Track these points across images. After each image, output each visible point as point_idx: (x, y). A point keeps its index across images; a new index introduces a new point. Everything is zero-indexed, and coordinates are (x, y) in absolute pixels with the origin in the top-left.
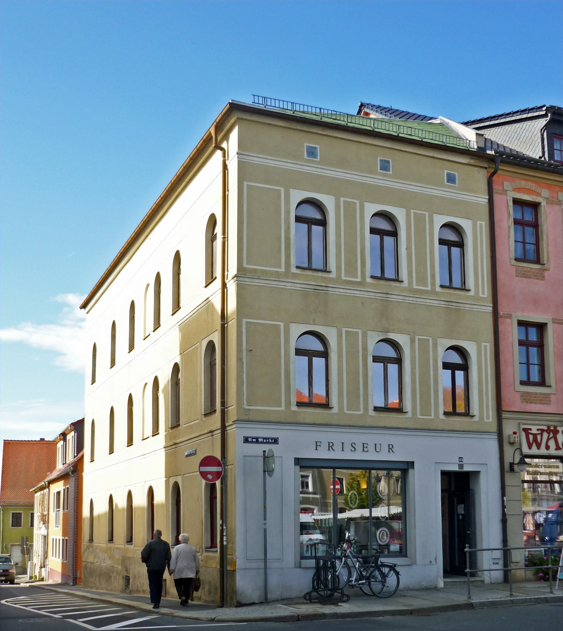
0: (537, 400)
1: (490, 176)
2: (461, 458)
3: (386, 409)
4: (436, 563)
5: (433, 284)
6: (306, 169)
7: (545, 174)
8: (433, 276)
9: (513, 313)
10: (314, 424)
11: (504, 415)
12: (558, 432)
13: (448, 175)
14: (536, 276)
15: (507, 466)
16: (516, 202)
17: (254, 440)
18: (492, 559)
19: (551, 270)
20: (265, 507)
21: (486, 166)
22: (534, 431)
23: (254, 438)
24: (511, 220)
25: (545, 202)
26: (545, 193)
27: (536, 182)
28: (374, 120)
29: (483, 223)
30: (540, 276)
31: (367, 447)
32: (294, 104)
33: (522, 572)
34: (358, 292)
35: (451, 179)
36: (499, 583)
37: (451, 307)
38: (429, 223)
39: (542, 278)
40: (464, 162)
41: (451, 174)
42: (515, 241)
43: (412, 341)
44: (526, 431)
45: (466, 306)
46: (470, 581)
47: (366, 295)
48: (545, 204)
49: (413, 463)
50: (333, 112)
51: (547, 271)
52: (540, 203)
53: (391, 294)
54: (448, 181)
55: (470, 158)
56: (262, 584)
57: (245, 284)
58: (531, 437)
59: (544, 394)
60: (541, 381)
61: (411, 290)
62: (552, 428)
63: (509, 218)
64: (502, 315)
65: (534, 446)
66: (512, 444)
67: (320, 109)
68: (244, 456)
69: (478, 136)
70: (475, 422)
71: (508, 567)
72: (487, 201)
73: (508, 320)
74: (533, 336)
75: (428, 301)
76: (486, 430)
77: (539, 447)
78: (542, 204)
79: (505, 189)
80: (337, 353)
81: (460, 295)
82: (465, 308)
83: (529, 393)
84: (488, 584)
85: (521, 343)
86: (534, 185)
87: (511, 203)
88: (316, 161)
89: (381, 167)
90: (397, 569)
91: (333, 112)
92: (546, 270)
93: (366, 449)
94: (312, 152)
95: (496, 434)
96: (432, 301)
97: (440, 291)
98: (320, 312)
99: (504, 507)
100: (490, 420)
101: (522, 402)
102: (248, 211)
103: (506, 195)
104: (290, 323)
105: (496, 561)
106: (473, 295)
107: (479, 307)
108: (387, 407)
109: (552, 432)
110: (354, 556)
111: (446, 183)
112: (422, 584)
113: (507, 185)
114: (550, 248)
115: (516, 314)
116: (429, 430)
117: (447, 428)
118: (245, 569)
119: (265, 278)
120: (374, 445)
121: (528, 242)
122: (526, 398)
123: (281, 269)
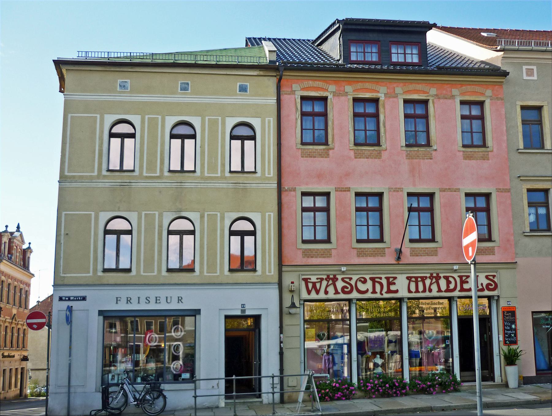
0: (376, 254)
2: (243, 304)
3: (181, 270)
4: (218, 388)
6: (118, 98)
7: (346, 74)
10: (116, 285)
11: (284, 269)
12: (337, 279)
14: (319, 155)
17: (67, 299)
20: (70, 348)
22: (314, 279)
23: (67, 297)
26: (332, 88)
27: (324, 81)
28: (175, 54)
29: (272, 119)
30: (326, 155)
31: (159, 300)
32: (110, 53)
34: (157, 184)
35: (243, 89)
37: (239, 187)
39: (328, 156)
40: (255, 74)
42: (462, 132)
43: (202, 217)
44: (306, 281)
45: (252, 185)
47: (163, 185)
49: (200, 310)
50: (141, 54)
52: (327, 97)
53: (185, 183)
54: (240, 91)
56: (66, 405)
57: (65, 187)
58: (310, 286)
59: (326, 249)
61: (203, 178)
63: (296, 112)
65: (313, 292)
66: (291, 291)
67: (130, 53)
69: (271, 53)
70: (258, 276)
73: (293, 193)
75: (218, 185)
76: (268, 281)
77: (318, 292)
80: (137, 231)
81: (246, 177)
82: (252, 187)
83: (310, 250)
84: (266, 404)
88: (127, 91)
89: (181, 88)
90: (165, 393)
91: (141, 54)
92: (330, 149)
93: (158, 302)
94: (123, 86)
95: (277, 284)
96: (221, 185)
97: (229, 176)
98: (124, 202)
100: (272, 273)
101: (304, 257)
102: (71, 134)
103: (294, 94)
107: (264, 185)
108: (181, 268)
110: (130, 383)
111: (238, 92)
112: (205, 404)
113: (295, 87)
114: (335, 131)
117: (231, 282)
118: (56, 393)
119: (81, 181)
120: (138, 298)
121: (475, 131)
122: (307, 254)
123: (94, 173)
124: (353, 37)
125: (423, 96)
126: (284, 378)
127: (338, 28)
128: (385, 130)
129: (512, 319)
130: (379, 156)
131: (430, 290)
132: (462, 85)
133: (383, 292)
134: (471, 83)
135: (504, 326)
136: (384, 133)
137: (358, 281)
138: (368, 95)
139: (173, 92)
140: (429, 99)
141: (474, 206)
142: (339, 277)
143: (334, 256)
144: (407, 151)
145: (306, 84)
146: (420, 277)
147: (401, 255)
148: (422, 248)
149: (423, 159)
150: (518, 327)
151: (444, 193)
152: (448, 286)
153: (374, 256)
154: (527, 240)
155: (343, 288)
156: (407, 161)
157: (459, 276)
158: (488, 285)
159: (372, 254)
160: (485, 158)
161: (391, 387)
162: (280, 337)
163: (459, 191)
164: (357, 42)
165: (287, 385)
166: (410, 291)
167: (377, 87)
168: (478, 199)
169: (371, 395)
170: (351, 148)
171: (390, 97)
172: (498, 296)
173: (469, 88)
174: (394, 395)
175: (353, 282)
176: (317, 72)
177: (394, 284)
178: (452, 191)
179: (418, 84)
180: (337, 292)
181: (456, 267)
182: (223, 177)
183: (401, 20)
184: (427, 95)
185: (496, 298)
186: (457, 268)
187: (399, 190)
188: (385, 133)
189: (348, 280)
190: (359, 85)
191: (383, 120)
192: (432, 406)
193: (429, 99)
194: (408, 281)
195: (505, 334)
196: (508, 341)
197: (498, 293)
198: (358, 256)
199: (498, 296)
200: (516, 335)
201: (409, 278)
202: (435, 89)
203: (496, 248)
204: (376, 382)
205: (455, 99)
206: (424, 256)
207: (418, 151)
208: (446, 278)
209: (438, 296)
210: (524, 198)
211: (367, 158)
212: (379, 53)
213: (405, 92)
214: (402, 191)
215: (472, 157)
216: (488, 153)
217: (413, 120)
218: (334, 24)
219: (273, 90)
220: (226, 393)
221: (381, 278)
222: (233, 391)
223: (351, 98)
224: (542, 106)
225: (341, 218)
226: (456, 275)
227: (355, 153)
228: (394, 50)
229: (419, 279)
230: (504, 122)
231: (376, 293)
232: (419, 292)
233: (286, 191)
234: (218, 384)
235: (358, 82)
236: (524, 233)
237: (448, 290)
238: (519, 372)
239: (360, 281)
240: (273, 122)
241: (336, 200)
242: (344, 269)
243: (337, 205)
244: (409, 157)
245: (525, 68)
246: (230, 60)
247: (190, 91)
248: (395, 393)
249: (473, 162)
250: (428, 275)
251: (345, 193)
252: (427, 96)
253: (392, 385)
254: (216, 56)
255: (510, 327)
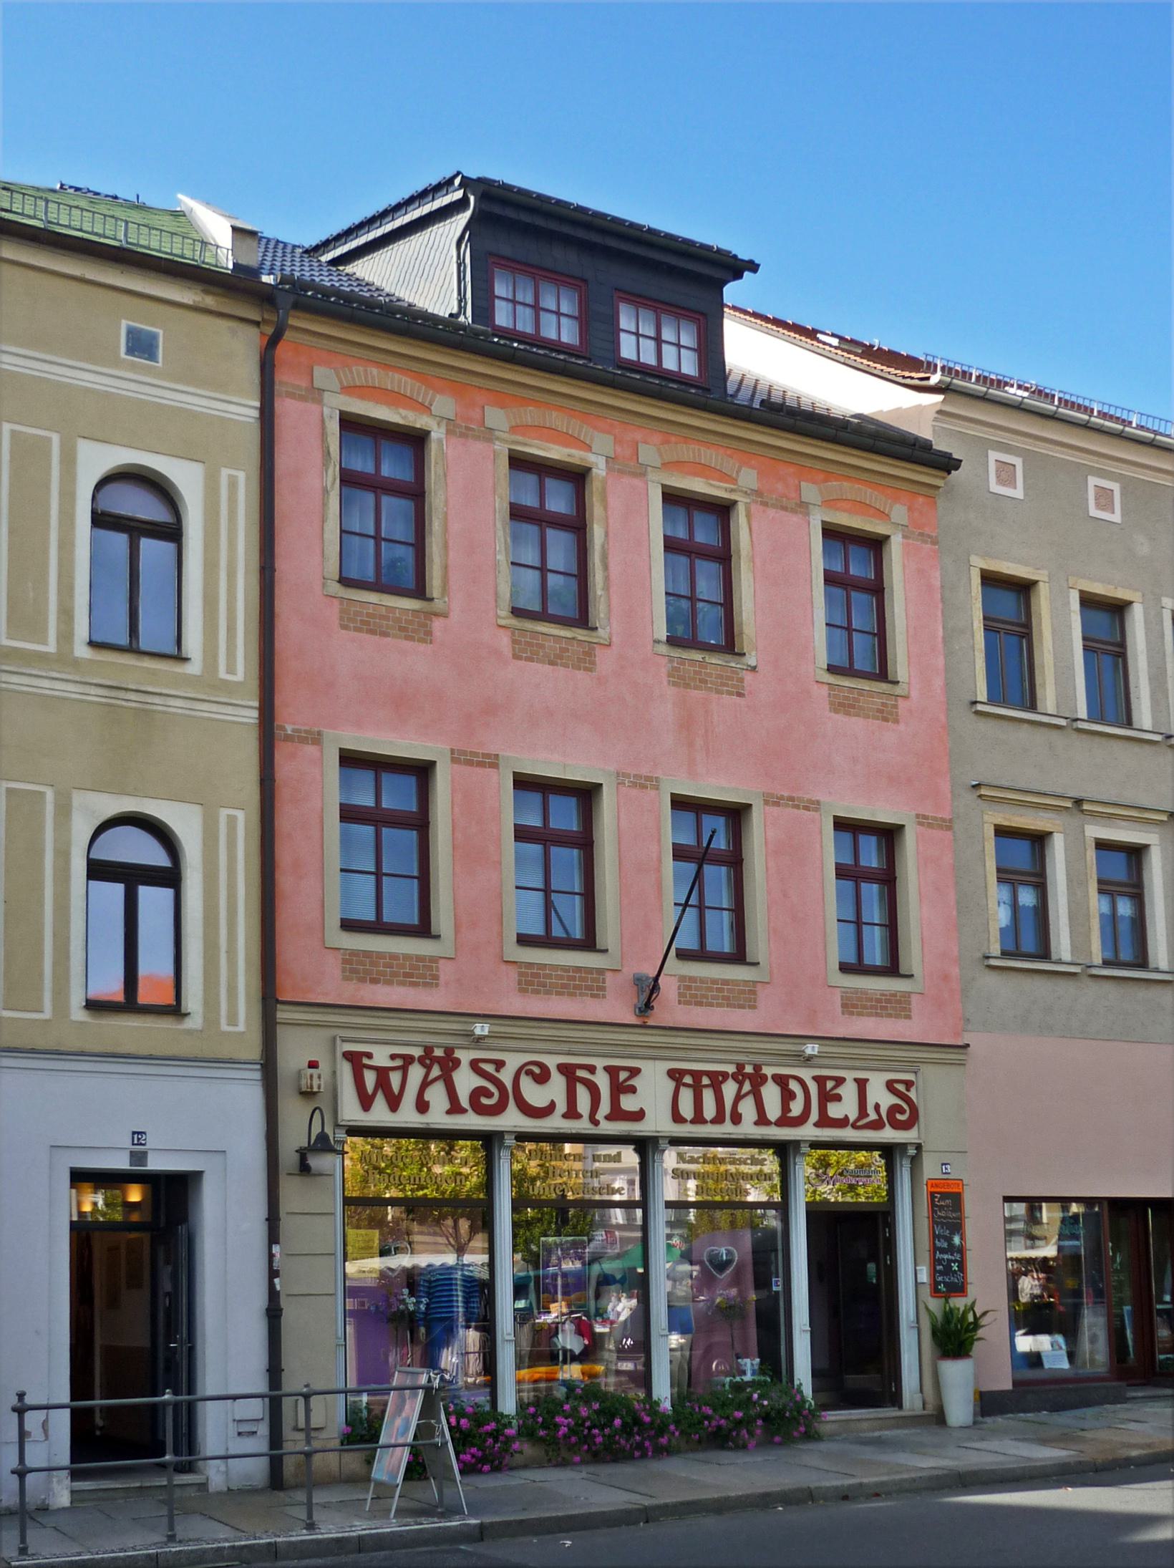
0: (579, 987)
1: (266, 348)
2: (139, 1133)
5: (66, 636)
8: (66, 614)
9: (325, 731)
11: (283, 1014)
12: (457, 1063)
13: (131, 332)
14: (401, 629)
15: (288, 1156)
16: (350, 424)
18: (234, 1420)
19: (455, 615)
21: (256, 317)
22: (381, 1057)
24: (333, 472)
25: (443, 430)
26: (444, 405)
27: (418, 376)
29: (241, 476)
30: (419, 630)
33: (333, 1458)
35: (141, 345)
36: (253, 1491)
37: (124, 703)
38: (61, 462)
39: (427, 636)
41: (140, 331)
44: (356, 1060)
46: (175, 1485)
48: (443, 436)
51: (441, 619)
52: (428, 433)
54: (130, 351)
55: (203, 291)
58: (370, 1079)
59: (420, 958)
60: (584, 938)
62: (439, 1053)
64: (289, 732)
65: (380, 1103)
66: (308, 1094)
68: (52, 1146)
69: (239, 236)
70: (189, 1032)
71: (434, 1438)
72: (256, 414)
73: (310, 750)
74: (871, 857)
75: (46, 683)
77: (394, 1103)
78: (434, 435)
79: (316, 384)
81: (154, 673)
83: (367, 954)
84: (219, 1493)
85: (842, 872)
86: (409, 380)
87: (334, 427)
92: (436, 615)
95: (258, 1067)
96: (58, 685)
99: (273, 1273)
100: (241, 1027)
101: (346, 979)
103: (320, 401)
104: (74, 790)
105: (245, 1428)
106: (199, 674)
107: (214, 708)
109: (439, 1063)
113: (322, 375)
114: (451, 554)
115: (337, 732)
116: (33, 1051)
122: (357, 967)
124: (506, 250)
125: (718, 487)
126: (285, 1400)
127: (460, 205)
128: (607, 579)
129: (954, 1218)
130: (586, 660)
131: (737, 1119)
132: (829, 476)
133: (600, 1115)
134: (852, 473)
135: (934, 1237)
136: (603, 589)
137: (523, 1072)
138: (555, 452)
139: (95, 353)
140: (735, 502)
141: (373, 805)
142: (465, 1056)
143: (447, 984)
144: (671, 659)
145: (358, 374)
146: (708, 1073)
147: (654, 995)
148: (714, 981)
149: (719, 692)
150: (970, 1243)
151: (775, 810)
152: (786, 1108)
153: (572, 995)
154: (992, 980)
155: (477, 1093)
156: (671, 691)
157: (815, 1078)
158: (894, 1109)
159: (564, 986)
160: (887, 715)
161: (626, 1429)
162: (271, 1256)
163: (817, 810)
164: (516, 266)
165: (293, 1424)
166: (677, 1118)
167: (586, 432)
168: (555, 801)
169: (564, 1453)
170: (502, 622)
171: (621, 472)
172: (919, 1147)
173: (848, 489)
174: (637, 1454)
175: (506, 1077)
176: (346, 325)
177: (633, 1090)
178: (797, 807)
179: (708, 444)
180: (455, 1108)
181: (811, 1049)
182: (64, 659)
183: (580, 204)
184: (732, 486)
185: (912, 1152)
186: (816, 1053)
187: (646, 783)
188: (607, 587)
189: (490, 1068)
190: (530, 415)
191: (603, 547)
192: (812, 1486)
193: (735, 502)
194: (671, 1085)
195: (935, 1262)
196: (944, 1283)
197: (919, 1138)
198: (523, 991)
199: (919, 1147)
200: (962, 1267)
201: (676, 1075)
202: (754, 473)
203: (914, 999)
204: (584, 1411)
205: (808, 514)
206: (719, 1005)
207: (703, 664)
208: (781, 1081)
209: (759, 1137)
210: (986, 852)
211: (552, 663)
212: (585, 320)
213: (667, 466)
214: (657, 788)
215: (853, 707)
216: (896, 701)
217: (370, 498)
218: (444, 186)
219: (249, 371)
220: (73, 1460)
221: (592, 1069)
222: (163, 1443)
223: (502, 449)
224: (1035, 583)
225: (469, 855)
226: (806, 1074)
227: (514, 642)
228: (626, 322)
229: (706, 1081)
230: (939, 614)
231: (578, 1116)
232: (704, 1121)
233: (288, 738)
234: (45, 1425)
235: (526, 402)
236: (988, 958)
237: (785, 1121)
238: (977, 1377)
239: (529, 1073)
240: (247, 485)
241: (453, 791)
242: (481, 1029)
243: (456, 809)
244: (679, 679)
245: (1093, 481)
246: (87, 227)
247: (160, 365)
248: (639, 1446)
249: (856, 725)
250: (731, 1069)
251: (479, 770)
252: (732, 491)
253: (629, 1420)
254: (127, 222)
255: (949, 1240)
